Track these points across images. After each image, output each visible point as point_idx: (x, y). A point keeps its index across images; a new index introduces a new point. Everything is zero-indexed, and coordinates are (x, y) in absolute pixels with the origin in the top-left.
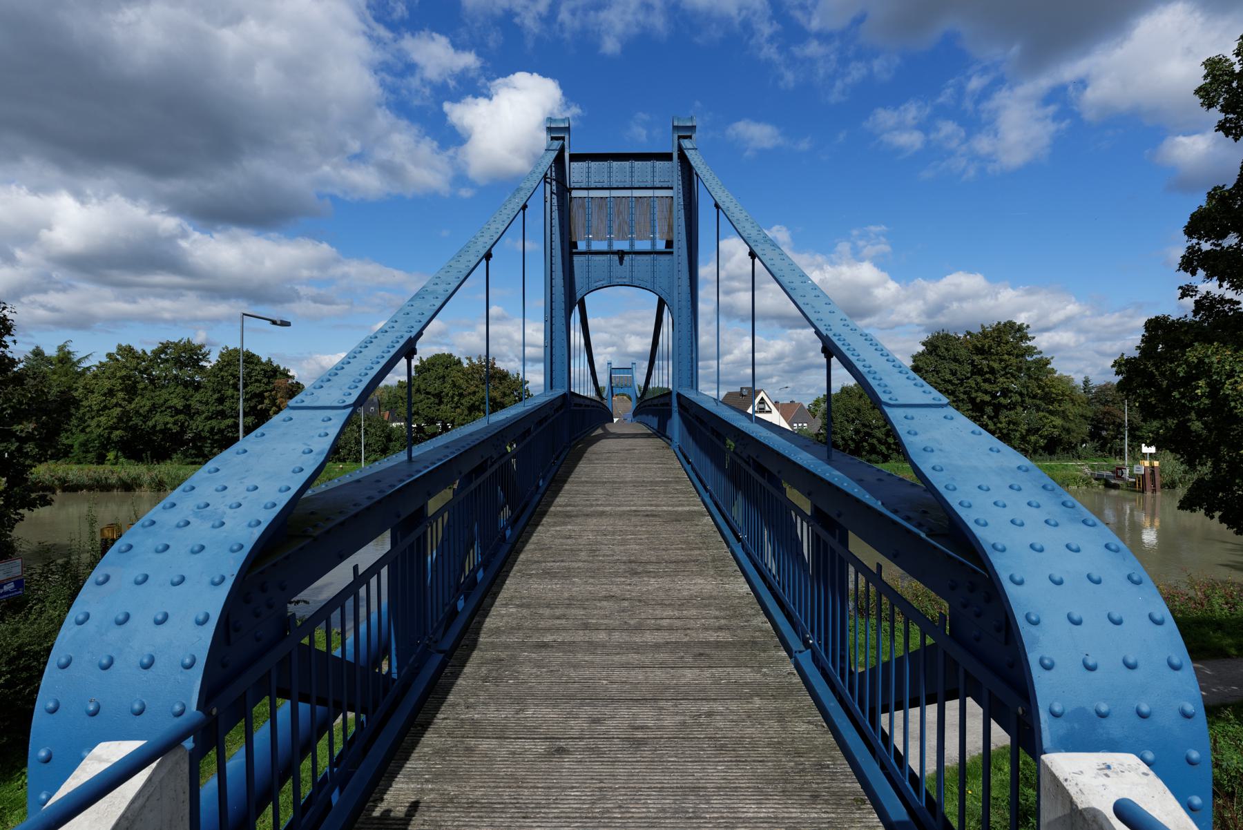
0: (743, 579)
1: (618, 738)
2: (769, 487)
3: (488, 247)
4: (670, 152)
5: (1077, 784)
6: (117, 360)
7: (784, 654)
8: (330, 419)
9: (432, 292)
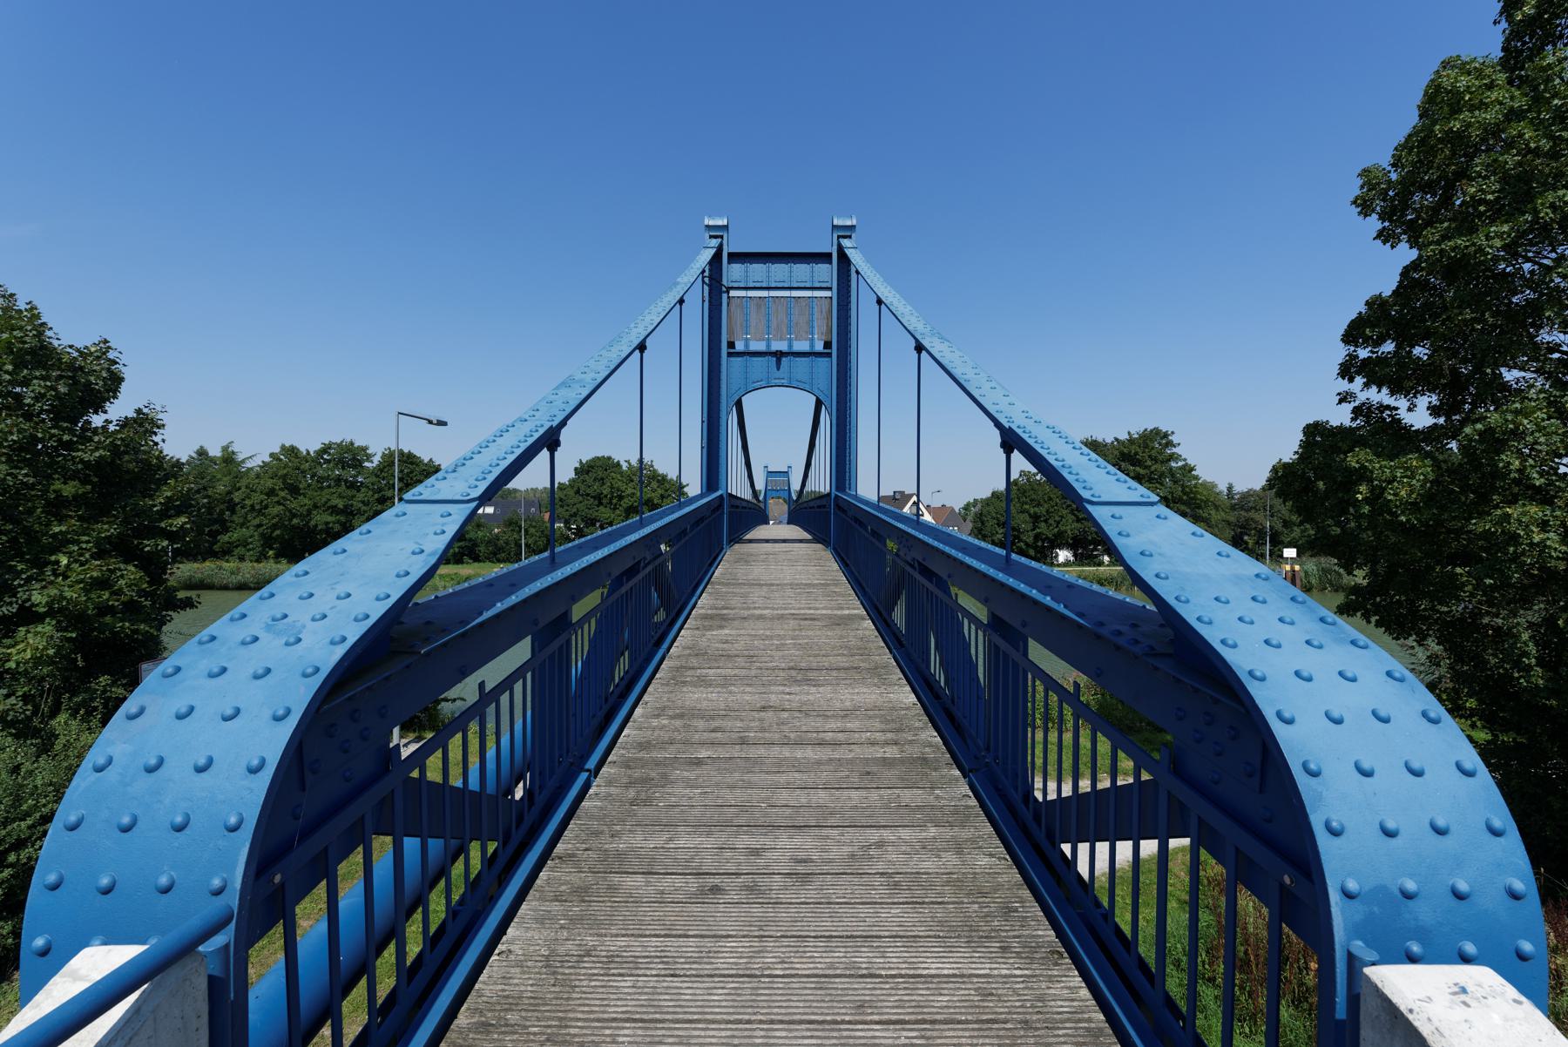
0: (908, 688)
1: (779, 874)
2: (937, 592)
3: (642, 338)
4: (828, 251)
5: (1429, 1019)
6: (281, 460)
7: (957, 773)
8: (450, 515)
9: (580, 381)
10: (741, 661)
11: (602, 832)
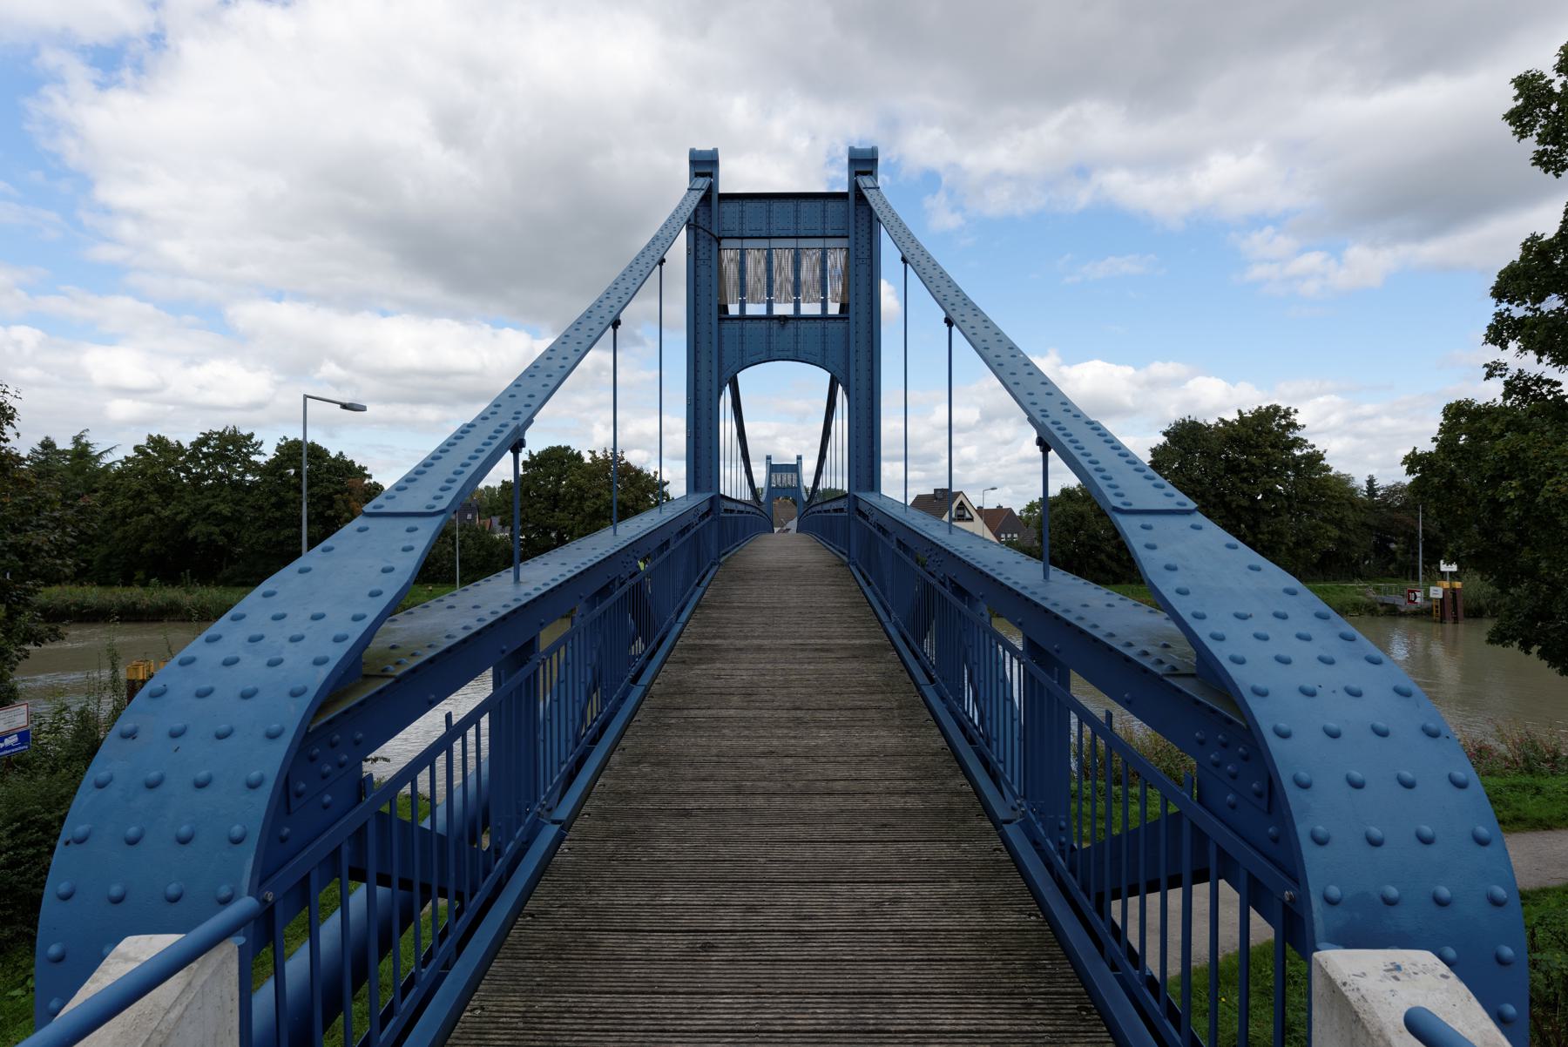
3: (615, 312)
10: (736, 700)
11: (578, 889)
